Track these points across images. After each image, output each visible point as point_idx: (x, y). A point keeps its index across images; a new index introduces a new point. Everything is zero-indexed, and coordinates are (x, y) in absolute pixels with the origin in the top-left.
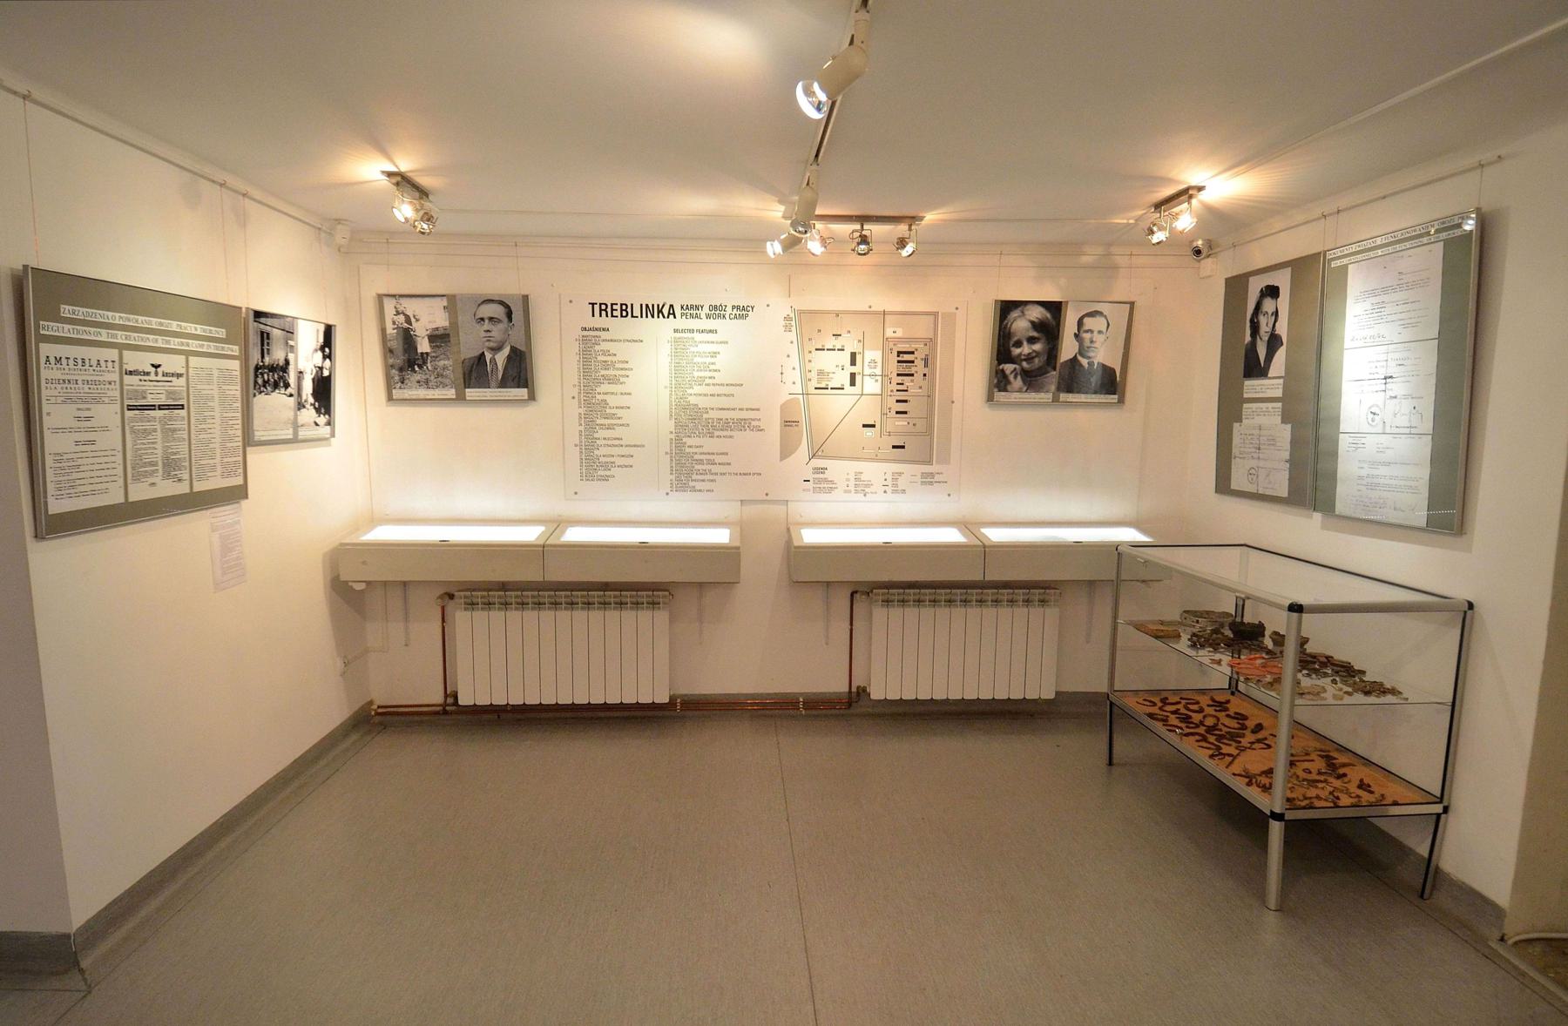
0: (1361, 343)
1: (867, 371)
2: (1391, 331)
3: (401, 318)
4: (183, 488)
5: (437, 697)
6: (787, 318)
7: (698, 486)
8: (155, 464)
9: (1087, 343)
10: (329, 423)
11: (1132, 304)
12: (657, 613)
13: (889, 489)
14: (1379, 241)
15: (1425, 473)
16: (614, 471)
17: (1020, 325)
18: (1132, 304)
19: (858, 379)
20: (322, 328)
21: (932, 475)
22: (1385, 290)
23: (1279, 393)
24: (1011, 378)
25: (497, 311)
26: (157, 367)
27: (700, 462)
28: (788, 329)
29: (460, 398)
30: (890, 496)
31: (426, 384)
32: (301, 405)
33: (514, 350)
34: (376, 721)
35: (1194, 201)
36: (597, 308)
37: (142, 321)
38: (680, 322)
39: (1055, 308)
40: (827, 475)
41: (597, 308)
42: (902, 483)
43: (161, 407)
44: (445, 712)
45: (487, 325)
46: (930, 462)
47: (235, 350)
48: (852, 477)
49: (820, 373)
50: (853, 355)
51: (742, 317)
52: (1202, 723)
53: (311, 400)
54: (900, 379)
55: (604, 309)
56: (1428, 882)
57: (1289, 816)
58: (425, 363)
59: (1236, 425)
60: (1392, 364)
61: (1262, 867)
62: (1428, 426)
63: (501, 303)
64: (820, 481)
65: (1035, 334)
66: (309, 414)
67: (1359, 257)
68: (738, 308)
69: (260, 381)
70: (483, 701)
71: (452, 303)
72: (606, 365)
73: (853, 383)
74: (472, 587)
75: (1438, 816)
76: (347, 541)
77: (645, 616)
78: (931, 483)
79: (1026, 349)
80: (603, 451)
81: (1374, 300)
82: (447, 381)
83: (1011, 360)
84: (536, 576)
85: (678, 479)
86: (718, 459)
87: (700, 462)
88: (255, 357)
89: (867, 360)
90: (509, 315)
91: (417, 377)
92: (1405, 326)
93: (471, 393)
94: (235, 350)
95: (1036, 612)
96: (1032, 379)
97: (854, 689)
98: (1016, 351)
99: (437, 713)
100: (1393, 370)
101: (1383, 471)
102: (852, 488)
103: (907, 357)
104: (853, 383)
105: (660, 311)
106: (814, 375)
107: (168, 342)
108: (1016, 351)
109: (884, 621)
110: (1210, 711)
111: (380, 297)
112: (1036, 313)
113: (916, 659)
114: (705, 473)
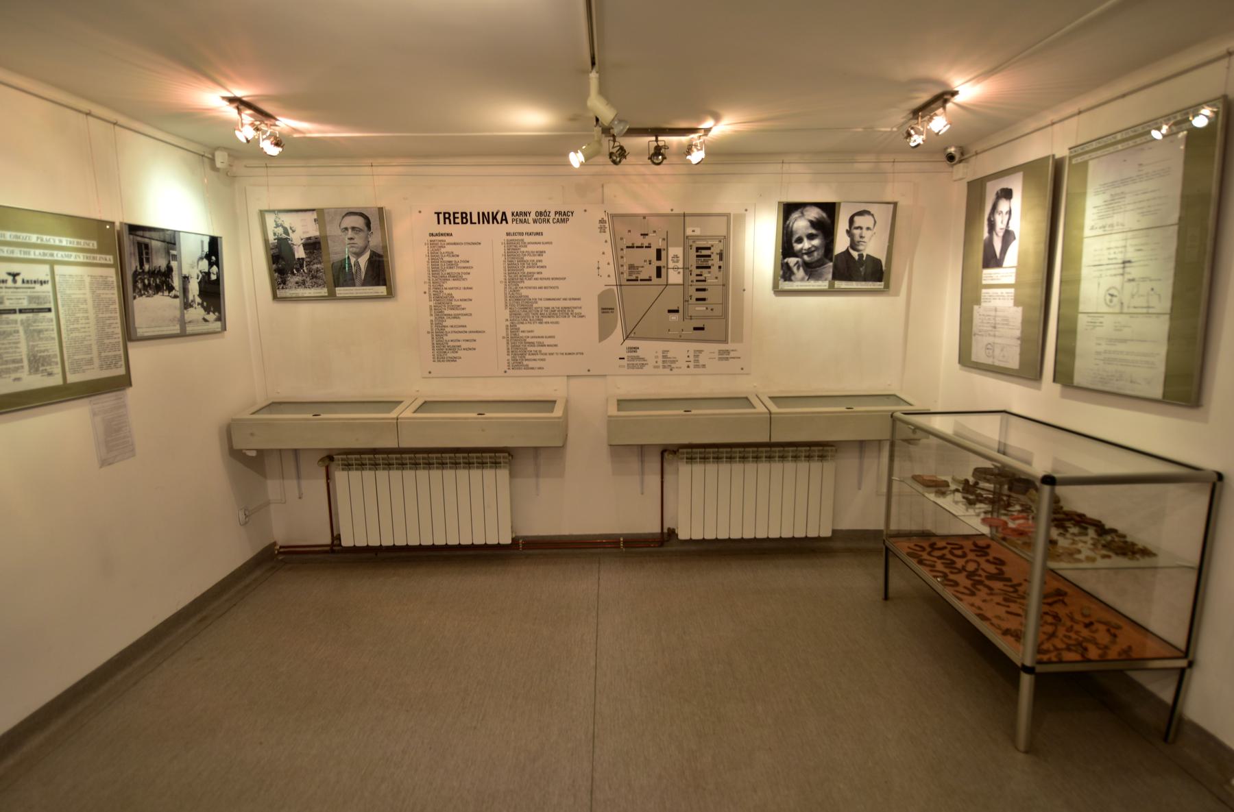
0: (1101, 232)
1: (671, 265)
2: (1128, 218)
3: (280, 230)
4: (56, 381)
5: (327, 540)
6: (602, 221)
7: (531, 364)
8: (21, 361)
9: (857, 238)
10: (219, 319)
11: (895, 204)
12: (498, 471)
13: (691, 364)
14: (1119, 137)
15: (1163, 350)
16: (460, 353)
17: (801, 224)
18: (895, 204)
19: (663, 271)
20: (207, 240)
21: (728, 352)
22: (1124, 182)
23: (1012, 280)
24: (795, 269)
25: (358, 222)
26: (14, 275)
27: (532, 344)
28: (602, 230)
29: (332, 296)
30: (692, 370)
31: (302, 284)
32: (187, 305)
33: (373, 254)
34: (277, 561)
35: (949, 106)
36: (441, 216)
37: (24, 237)
38: (512, 227)
39: (830, 209)
40: (639, 353)
41: (441, 216)
42: (703, 359)
43: (21, 311)
44: (333, 551)
45: (350, 233)
46: (726, 341)
47: (110, 259)
48: (660, 355)
49: (631, 267)
50: (659, 252)
51: (563, 221)
52: (964, 568)
53: (198, 300)
54: (698, 272)
55: (448, 217)
56: (1170, 729)
57: (1039, 669)
58: (302, 266)
59: (976, 307)
60: (1130, 249)
61: (1015, 702)
62: (1165, 304)
63: (361, 215)
64: (633, 358)
65: (813, 231)
66: (197, 313)
67: (1099, 153)
68: (560, 213)
69: (140, 285)
70: (361, 543)
71: (321, 215)
72: (451, 265)
73: (659, 275)
74: (348, 452)
75: (1182, 671)
76: (238, 417)
77: (489, 473)
78: (727, 359)
79: (806, 244)
80: (451, 337)
81: (1113, 191)
82: (320, 282)
83: (795, 255)
84: (392, 444)
85: (514, 359)
86: (547, 341)
87: (532, 344)
88: (133, 264)
89: (671, 254)
90: (368, 224)
91: (297, 279)
92: (1143, 214)
93: (341, 291)
94: (110, 259)
95: (816, 466)
96: (812, 269)
97: (665, 530)
98: (798, 247)
99: (326, 552)
100: (1131, 255)
101: (1121, 347)
102: (660, 363)
103: (704, 252)
104: (659, 275)
105: (494, 218)
106: (625, 268)
107: (45, 254)
108: (798, 247)
109: (686, 475)
110: (971, 556)
111: (262, 213)
112: (814, 214)
113: (713, 505)
114: (536, 353)
